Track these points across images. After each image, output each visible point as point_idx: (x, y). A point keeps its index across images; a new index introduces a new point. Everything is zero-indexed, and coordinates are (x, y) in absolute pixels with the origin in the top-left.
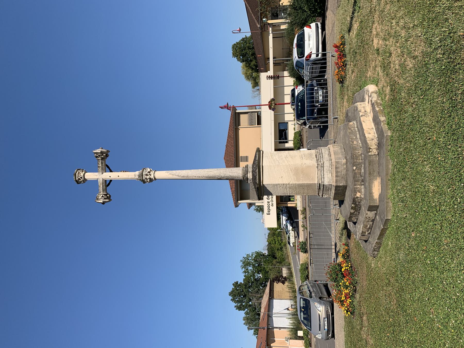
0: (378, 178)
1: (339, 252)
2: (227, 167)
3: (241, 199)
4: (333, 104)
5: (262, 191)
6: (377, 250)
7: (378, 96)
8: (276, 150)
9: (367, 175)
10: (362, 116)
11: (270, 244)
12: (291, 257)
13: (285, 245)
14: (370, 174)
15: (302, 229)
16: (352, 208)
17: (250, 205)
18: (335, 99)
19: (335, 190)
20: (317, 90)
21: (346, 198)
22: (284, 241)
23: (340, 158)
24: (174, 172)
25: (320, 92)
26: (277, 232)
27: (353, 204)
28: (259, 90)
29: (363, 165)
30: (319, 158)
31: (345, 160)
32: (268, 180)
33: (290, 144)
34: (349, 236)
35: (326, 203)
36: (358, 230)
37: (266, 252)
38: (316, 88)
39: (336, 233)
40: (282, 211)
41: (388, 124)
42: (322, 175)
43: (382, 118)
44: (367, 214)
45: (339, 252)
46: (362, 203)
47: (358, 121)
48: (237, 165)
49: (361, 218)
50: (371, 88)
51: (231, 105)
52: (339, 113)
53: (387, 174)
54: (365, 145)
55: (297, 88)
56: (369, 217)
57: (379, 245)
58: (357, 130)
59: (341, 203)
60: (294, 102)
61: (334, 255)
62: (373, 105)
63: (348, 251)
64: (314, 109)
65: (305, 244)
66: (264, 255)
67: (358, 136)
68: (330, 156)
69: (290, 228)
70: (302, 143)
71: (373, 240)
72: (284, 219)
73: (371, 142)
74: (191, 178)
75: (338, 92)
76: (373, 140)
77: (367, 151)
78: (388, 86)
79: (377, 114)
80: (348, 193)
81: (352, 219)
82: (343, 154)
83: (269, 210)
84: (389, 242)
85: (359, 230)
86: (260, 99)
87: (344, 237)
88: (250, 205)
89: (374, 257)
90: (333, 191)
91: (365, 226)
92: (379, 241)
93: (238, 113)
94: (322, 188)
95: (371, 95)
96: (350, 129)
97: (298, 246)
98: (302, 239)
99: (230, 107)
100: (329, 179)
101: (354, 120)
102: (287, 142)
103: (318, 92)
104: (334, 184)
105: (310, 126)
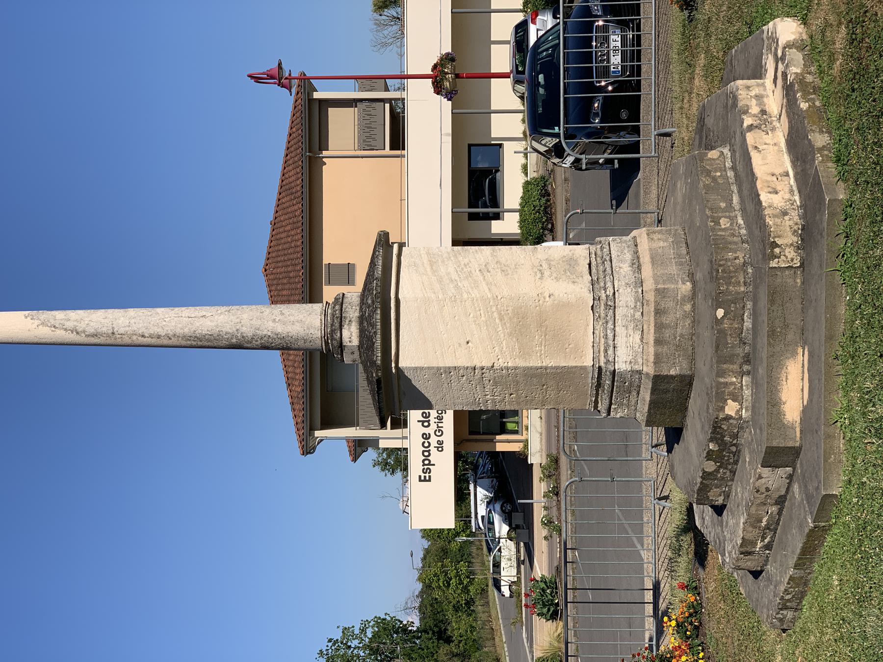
0: (800, 350)
1: (666, 613)
2: (274, 302)
3: (325, 425)
4: (657, 85)
5: (395, 396)
6: (794, 604)
7: (809, 60)
8: (455, 243)
9: (763, 340)
10: (751, 128)
11: (428, 587)
12: (502, 636)
13: (484, 592)
14: (772, 334)
15: (545, 532)
16: (710, 456)
17: (358, 447)
18: (663, 64)
19: (654, 391)
20: (605, 29)
21: (689, 421)
22: (479, 577)
23: (671, 279)
24: (59, 315)
25: (615, 40)
26: (454, 546)
27: (711, 440)
28: (399, 20)
29: (749, 305)
30: (599, 274)
31: (689, 285)
32: (416, 351)
33: (508, 224)
34: (701, 555)
35: (626, 437)
36: (729, 533)
37: (414, 620)
38: (601, 23)
39: (656, 545)
40: (475, 468)
41: (838, 161)
42: (610, 335)
43: (820, 139)
44: (760, 477)
45: (666, 613)
46: (745, 437)
47: (737, 148)
48: (312, 296)
49: (741, 492)
50: (787, 29)
51: (292, 68)
52: (677, 115)
53: (830, 338)
54: (757, 232)
55: (534, 22)
56: (768, 490)
57: (800, 585)
58: (732, 180)
59: (674, 436)
60: (523, 73)
61: (650, 625)
62: (789, 91)
63: (695, 610)
64: (591, 100)
65: (550, 585)
66: (405, 630)
67: (736, 199)
68: (639, 268)
69: (502, 529)
70: (550, 220)
71: (781, 572)
72: (480, 495)
73: (778, 221)
74: (126, 340)
75: (676, 39)
76: (785, 213)
77: (764, 254)
78: (840, 23)
79: (802, 122)
80: (695, 404)
81: (710, 493)
82: (681, 264)
83: (427, 465)
84: (832, 578)
85: (733, 533)
86: (401, 55)
87: (685, 560)
88: (358, 447)
89: (784, 631)
90: (646, 395)
91: (754, 521)
92: (799, 573)
93: (321, 101)
94: (607, 381)
95: (784, 54)
96: (708, 173)
97: (527, 595)
98: (541, 569)
99: (290, 78)
100: (631, 352)
101: (723, 144)
102: (497, 217)
103: (607, 39)
104: (649, 369)
105: (577, 161)
